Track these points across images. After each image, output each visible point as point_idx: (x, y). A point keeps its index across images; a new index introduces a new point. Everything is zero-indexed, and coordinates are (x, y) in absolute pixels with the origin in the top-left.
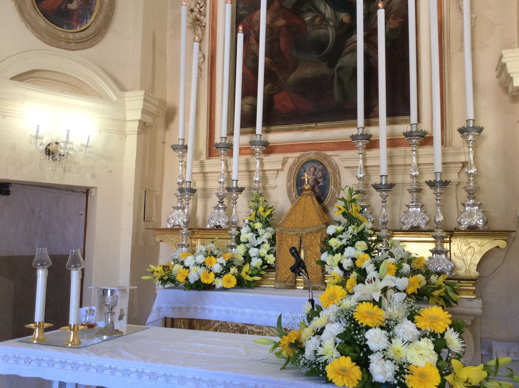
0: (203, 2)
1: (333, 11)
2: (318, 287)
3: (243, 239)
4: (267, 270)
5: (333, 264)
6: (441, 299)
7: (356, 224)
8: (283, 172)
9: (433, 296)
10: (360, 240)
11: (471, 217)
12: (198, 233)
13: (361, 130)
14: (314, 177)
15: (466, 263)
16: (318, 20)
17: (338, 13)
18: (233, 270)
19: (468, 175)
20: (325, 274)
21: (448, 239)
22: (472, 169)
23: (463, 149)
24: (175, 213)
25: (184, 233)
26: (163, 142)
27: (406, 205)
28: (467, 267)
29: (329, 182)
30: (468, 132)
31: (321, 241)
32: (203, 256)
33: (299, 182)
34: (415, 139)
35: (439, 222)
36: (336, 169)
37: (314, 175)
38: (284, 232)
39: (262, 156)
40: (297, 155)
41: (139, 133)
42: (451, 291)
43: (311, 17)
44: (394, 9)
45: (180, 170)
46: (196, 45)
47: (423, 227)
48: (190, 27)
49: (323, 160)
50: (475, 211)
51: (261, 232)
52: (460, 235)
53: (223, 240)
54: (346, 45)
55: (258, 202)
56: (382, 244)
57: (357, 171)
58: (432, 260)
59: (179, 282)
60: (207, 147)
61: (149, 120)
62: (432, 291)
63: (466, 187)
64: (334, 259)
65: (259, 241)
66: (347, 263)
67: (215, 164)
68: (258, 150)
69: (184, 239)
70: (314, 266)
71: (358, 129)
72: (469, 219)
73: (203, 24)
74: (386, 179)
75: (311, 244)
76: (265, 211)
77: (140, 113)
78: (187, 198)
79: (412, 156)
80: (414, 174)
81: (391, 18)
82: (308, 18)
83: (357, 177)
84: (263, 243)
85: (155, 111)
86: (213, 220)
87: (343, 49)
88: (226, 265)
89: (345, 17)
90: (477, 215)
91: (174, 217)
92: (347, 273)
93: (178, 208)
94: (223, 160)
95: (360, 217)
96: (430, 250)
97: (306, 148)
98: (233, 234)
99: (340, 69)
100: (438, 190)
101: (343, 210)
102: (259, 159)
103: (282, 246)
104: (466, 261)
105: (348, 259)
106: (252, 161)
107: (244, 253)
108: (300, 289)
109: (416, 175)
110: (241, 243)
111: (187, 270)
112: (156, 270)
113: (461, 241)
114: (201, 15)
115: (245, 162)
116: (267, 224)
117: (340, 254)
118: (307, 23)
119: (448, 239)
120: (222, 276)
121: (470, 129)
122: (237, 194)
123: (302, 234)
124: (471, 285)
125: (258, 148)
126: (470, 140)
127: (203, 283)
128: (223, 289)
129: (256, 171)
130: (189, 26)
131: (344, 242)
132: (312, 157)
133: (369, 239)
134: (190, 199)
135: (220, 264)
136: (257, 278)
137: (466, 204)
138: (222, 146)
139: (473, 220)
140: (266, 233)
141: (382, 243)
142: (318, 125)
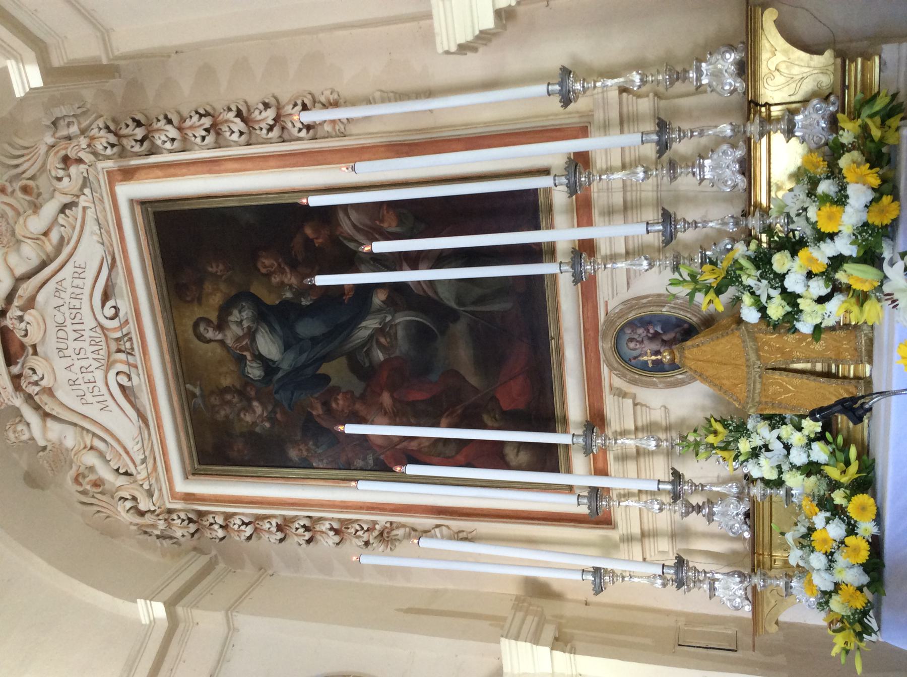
0: (353, 525)
1: (368, 317)
2: (866, 338)
3: (772, 475)
4: (834, 431)
5: (820, 313)
6: (888, 122)
7: (738, 272)
8: (637, 395)
9: (882, 138)
10: (771, 265)
11: (722, 73)
12: (760, 554)
13: (564, 268)
14: (646, 342)
15: (808, 74)
16: (382, 340)
17: (373, 309)
18: (838, 497)
19: (644, 85)
20: (840, 325)
21: (763, 109)
22: (634, 79)
23: (596, 96)
24: (721, 596)
25: (762, 583)
26: (586, 604)
27: (700, 184)
28: (816, 71)
29: (655, 315)
30: (569, 91)
31: (772, 334)
32: (813, 556)
33: (658, 367)
34: (580, 178)
35: (733, 130)
36: (630, 304)
37: (642, 342)
38: (757, 400)
39: (609, 432)
40: (605, 370)
41: (573, 651)
42: (872, 107)
43: (379, 352)
44: (368, 222)
45: (639, 582)
46: (425, 543)
47: (740, 152)
48: (393, 548)
49: (614, 328)
50: (710, 67)
51: (757, 442)
52: (755, 88)
53: (773, 510)
54: (422, 293)
55: (697, 444)
56: (776, 225)
57: (635, 270)
58: (807, 138)
59: (866, 604)
60: (594, 528)
61: (549, 632)
62: (872, 140)
63: (666, 86)
64: (809, 312)
65: (777, 446)
66: (818, 289)
67: (626, 515)
68: (600, 441)
69: (775, 584)
70: (824, 344)
71: (562, 273)
72: (724, 76)
73: (388, 525)
74: (653, 224)
75: (780, 350)
76: (715, 433)
77: (539, 647)
78: (695, 573)
79: (610, 180)
80: (641, 175)
81: (382, 225)
82: (379, 356)
83: (647, 270)
84: (779, 438)
85: (533, 620)
86: (734, 525)
87: (429, 298)
88: (828, 511)
89: (379, 298)
90: (717, 63)
91: (731, 598)
92: (837, 288)
93: (712, 589)
94: (619, 503)
95: (724, 265)
96: (787, 142)
97: (592, 355)
98: (762, 492)
99: (460, 302)
100: (674, 136)
101: (711, 295)
102: (616, 440)
103: (784, 403)
104: (805, 75)
105: (809, 286)
106: (620, 451)
107: (801, 475)
108: (871, 371)
109: (644, 172)
110: (780, 478)
111: (843, 586)
112: (843, 646)
113: (766, 85)
114: (374, 529)
115: (620, 463)
116: (741, 430)
117: (799, 301)
118: (387, 357)
119: (763, 109)
120: (852, 522)
121: (564, 89)
122: (685, 482)
123: (759, 367)
124: (853, 66)
125: (597, 441)
126: (583, 87)
127: (868, 558)
128: (879, 519)
129: (638, 444)
130: (391, 549)
131: (775, 293)
132: (610, 345)
133: (765, 245)
134: (695, 568)
135: (827, 523)
136: (853, 452)
137: (697, 84)
138: (594, 504)
139: (726, 71)
140: (759, 431)
141: (774, 223)
142: (552, 335)
